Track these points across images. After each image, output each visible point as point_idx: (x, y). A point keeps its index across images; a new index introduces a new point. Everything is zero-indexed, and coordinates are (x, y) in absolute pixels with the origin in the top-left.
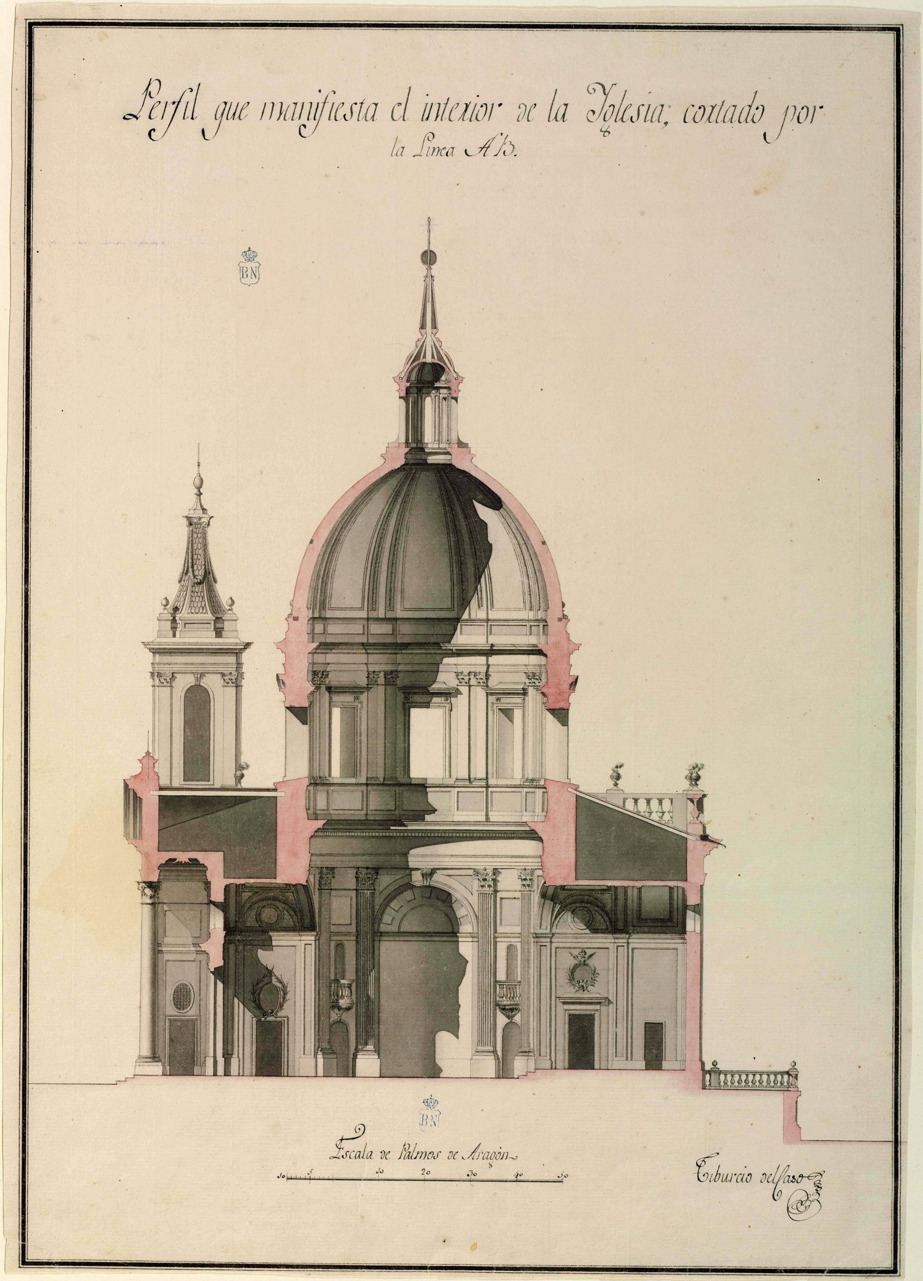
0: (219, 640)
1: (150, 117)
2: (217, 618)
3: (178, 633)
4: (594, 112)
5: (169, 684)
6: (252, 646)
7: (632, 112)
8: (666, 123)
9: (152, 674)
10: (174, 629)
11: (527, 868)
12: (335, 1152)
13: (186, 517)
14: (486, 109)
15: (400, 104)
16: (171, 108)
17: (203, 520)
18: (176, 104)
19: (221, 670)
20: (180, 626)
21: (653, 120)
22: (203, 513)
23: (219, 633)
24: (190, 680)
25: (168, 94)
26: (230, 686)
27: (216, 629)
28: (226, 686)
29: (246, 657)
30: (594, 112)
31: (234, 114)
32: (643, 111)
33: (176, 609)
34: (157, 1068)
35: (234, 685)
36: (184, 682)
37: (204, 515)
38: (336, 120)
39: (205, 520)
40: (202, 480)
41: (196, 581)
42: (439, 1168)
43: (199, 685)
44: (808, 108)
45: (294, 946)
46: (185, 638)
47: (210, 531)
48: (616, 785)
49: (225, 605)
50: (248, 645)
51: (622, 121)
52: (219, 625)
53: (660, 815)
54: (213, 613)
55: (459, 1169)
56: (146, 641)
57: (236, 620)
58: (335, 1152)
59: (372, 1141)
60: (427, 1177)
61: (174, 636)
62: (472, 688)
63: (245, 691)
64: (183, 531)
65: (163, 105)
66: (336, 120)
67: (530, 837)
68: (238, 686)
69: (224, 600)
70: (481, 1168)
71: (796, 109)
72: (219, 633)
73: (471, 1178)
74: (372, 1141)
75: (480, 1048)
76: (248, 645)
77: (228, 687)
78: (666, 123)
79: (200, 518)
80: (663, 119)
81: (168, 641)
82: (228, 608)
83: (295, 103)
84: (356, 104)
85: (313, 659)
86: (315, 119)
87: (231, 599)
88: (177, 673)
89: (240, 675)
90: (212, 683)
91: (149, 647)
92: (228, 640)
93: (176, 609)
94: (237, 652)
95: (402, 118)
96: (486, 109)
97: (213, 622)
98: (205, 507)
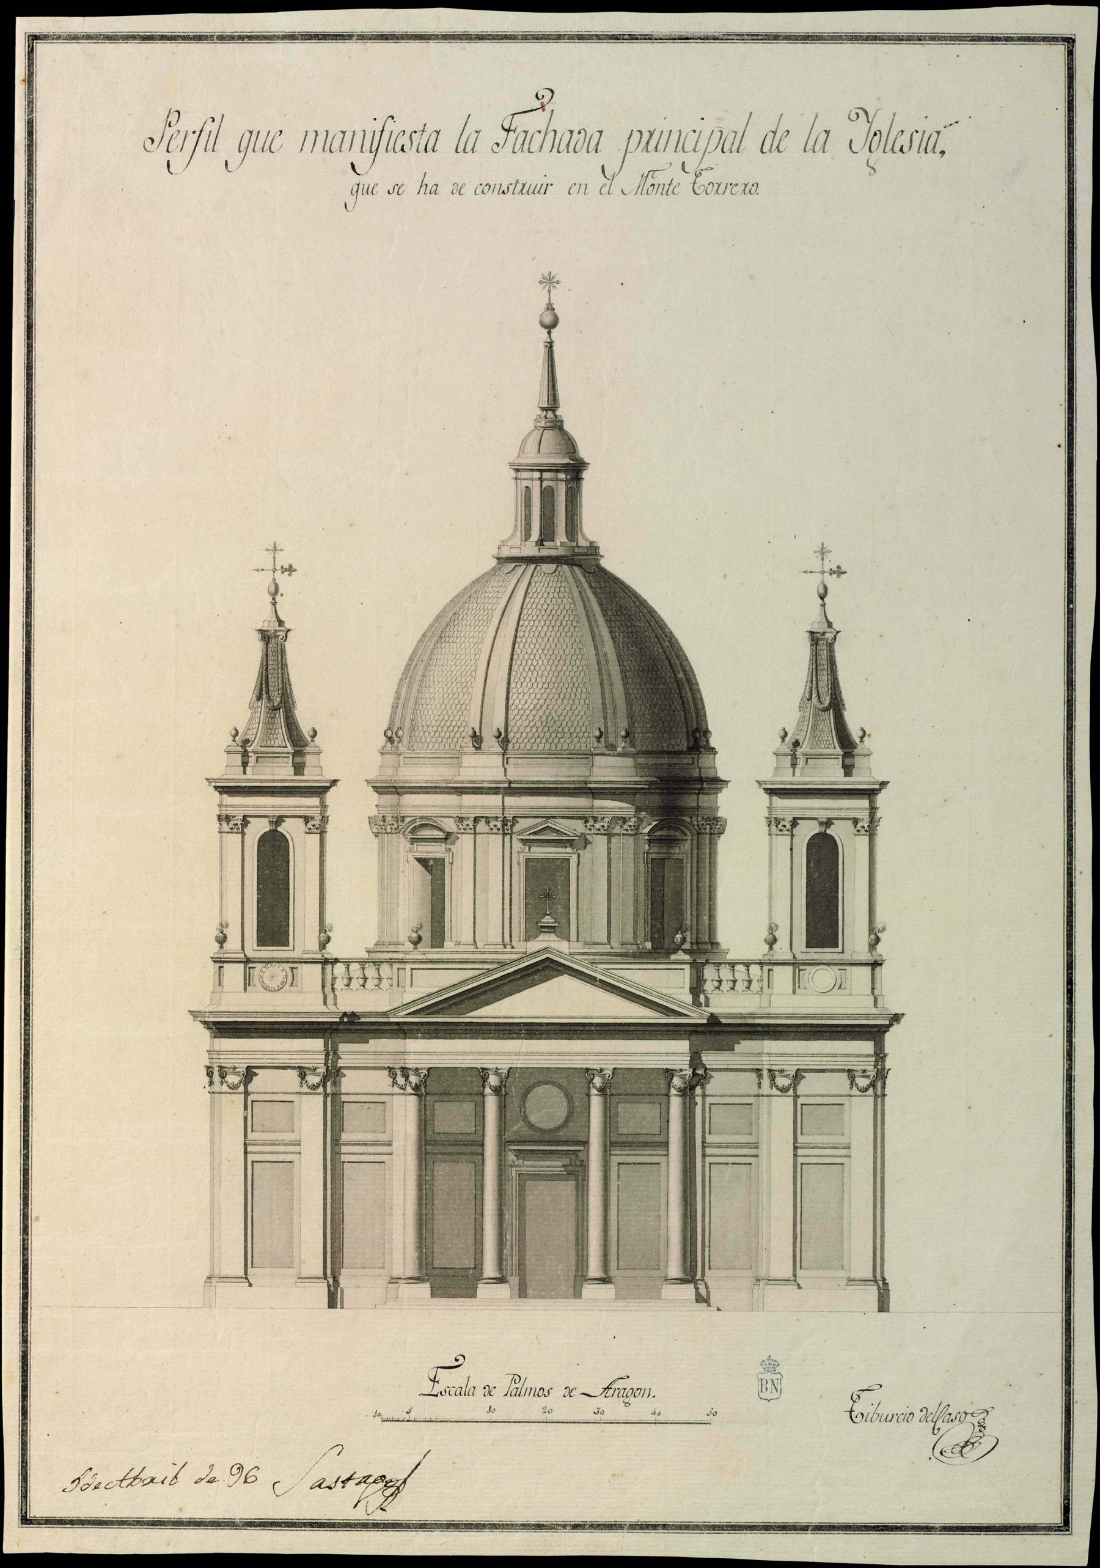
0: (848, 779)
1: (168, 151)
2: (845, 753)
4: (153, 141)
5: (789, 833)
7: (904, 140)
8: (943, 152)
9: (220, 818)
10: (245, 764)
12: (427, 1387)
13: (260, 630)
14: (586, 135)
15: (539, 132)
16: (192, 139)
18: (197, 133)
19: (853, 815)
20: (252, 760)
21: (590, 150)
22: (279, 626)
23: (299, 769)
24: (814, 829)
25: (189, 123)
26: (601, 834)
27: (844, 766)
29: (881, 799)
30: (153, 141)
31: (568, 145)
32: (917, 138)
33: (796, 744)
34: (424, 1289)
35: (868, 833)
36: (258, 828)
37: (830, 630)
38: (331, 151)
39: (829, 636)
40: (826, 589)
42: (562, 1408)
44: (586, 132)
47: (289, 646)
48: (221, 947)
50: (334, 782)
51: (779, 151)
52: (848, 761)
53: (716, 984)
54: (842, 746)
55: (585, 1408)
57: (319, 753)
58: (427, 1387)
59: (475, 1372)
60: (550, 1417)
61: (245, 773)
62: (478, 836)
64: (257, 648)
65: (182, 134)
66: (331, 151)
68: (322, 833)
70: (613, 1407)
71: (327, 135)
72: (848, 770)
73: (598, 1420)
74: (475, 1372)
76: (334, 782)
78: (943, 152)
80: (938, 149)
81: (788, 778)
82: (309, 739)
83: (342, 132)
84: (415, 132)
86: (240, 152)
89: (325, 820)
90: (291, 829)
91: (764, 786)
92: (859, 780)
94: (870, 794)
95: (822, 150)
96: (586, 135)
97: (841, 757)
98: (282, 618)
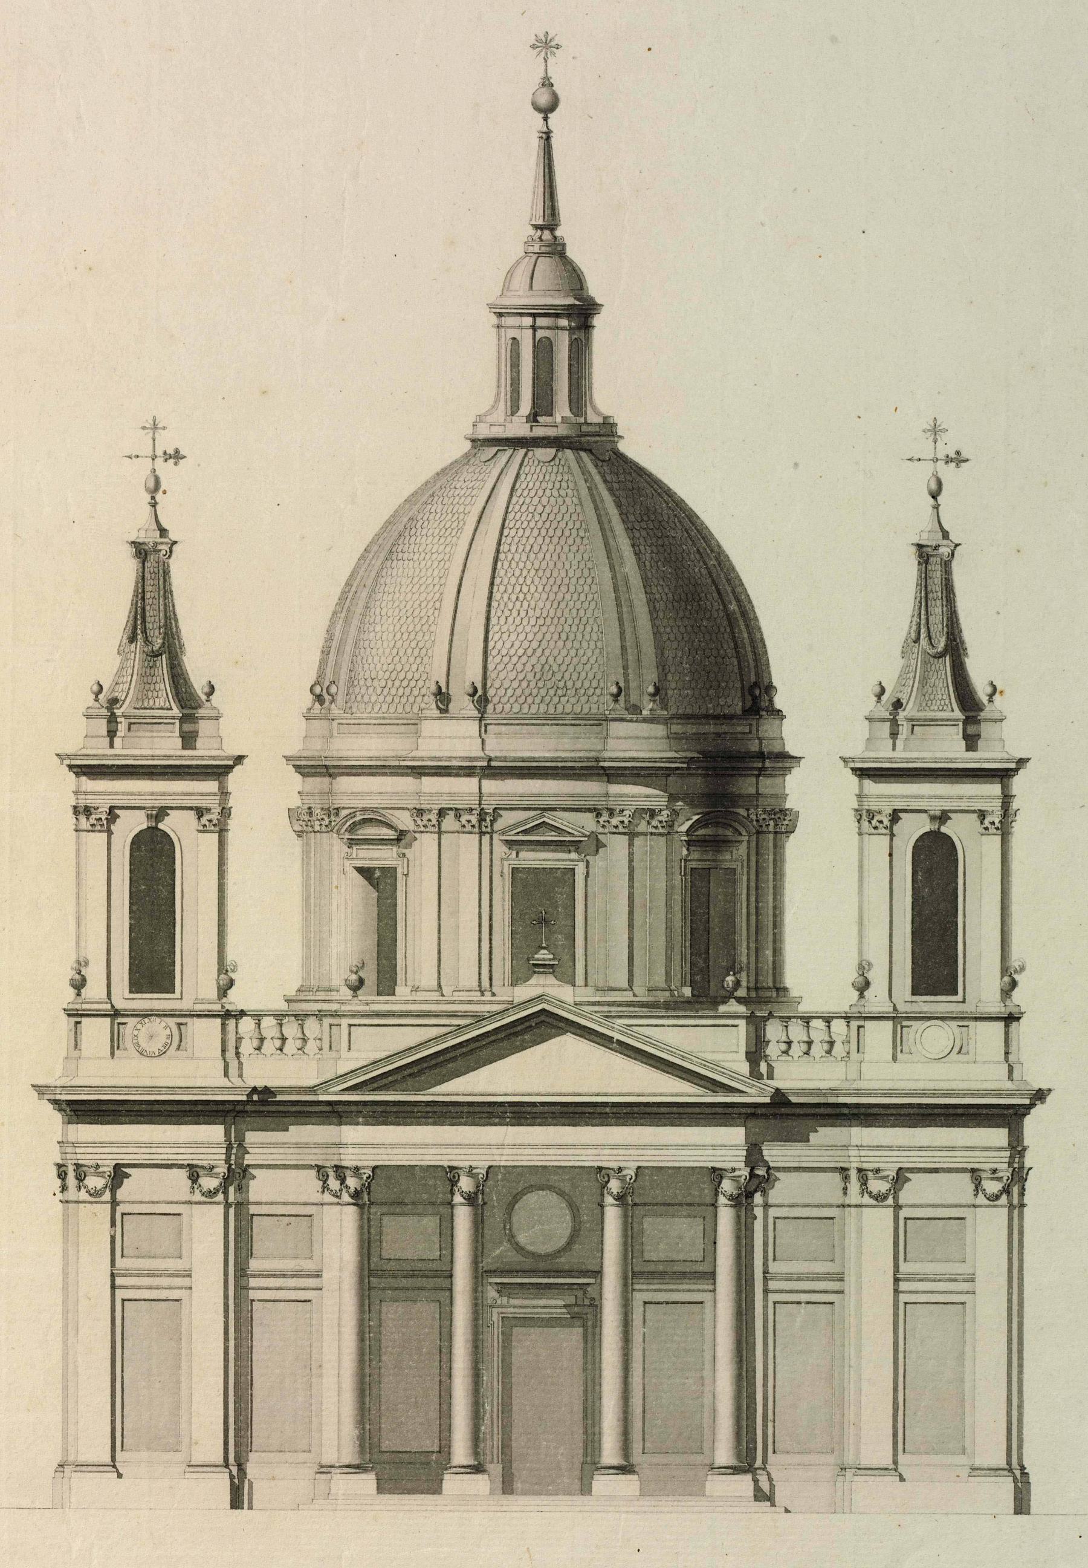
0: (971, 754)
2: (967, 718)
3: (117, 741)
5: (887, 832)
6: (245, 761)
10: (112, 734)
11: (100, 1162)
13: (133, 542)
17: (942, 550)
19: (978, 806)
22: (161, 536)
23: (189, 740)
26: (619, 833)
27: (966, 737)
28: (200, 831)
29: (1018, 783)
33: (898, 705)
40: (940, 483)
41: (932, 651)
43: (156, 828)
45: (963, 1303)
46: (905, 754)
49: (199, 692)
50: (239, 759)
52: (971, 730)
54: (963, 708)
56: (847, 755)
57: (217, 718)
61: (112, 746)
63: (230, 836)
64: (130, 567)
67: (956, 1108)
68: (222, 831)
69: (198, 685)
75: (246, 1505)
77: (427, 832)
79: (936, 547)
85: (78, 786)
87: (992, 683)
88: (501, 809)
90: (178, 825)
91: (852, 765)
93: (898, 705)
97: (961, 724)
98: (165, 525)
